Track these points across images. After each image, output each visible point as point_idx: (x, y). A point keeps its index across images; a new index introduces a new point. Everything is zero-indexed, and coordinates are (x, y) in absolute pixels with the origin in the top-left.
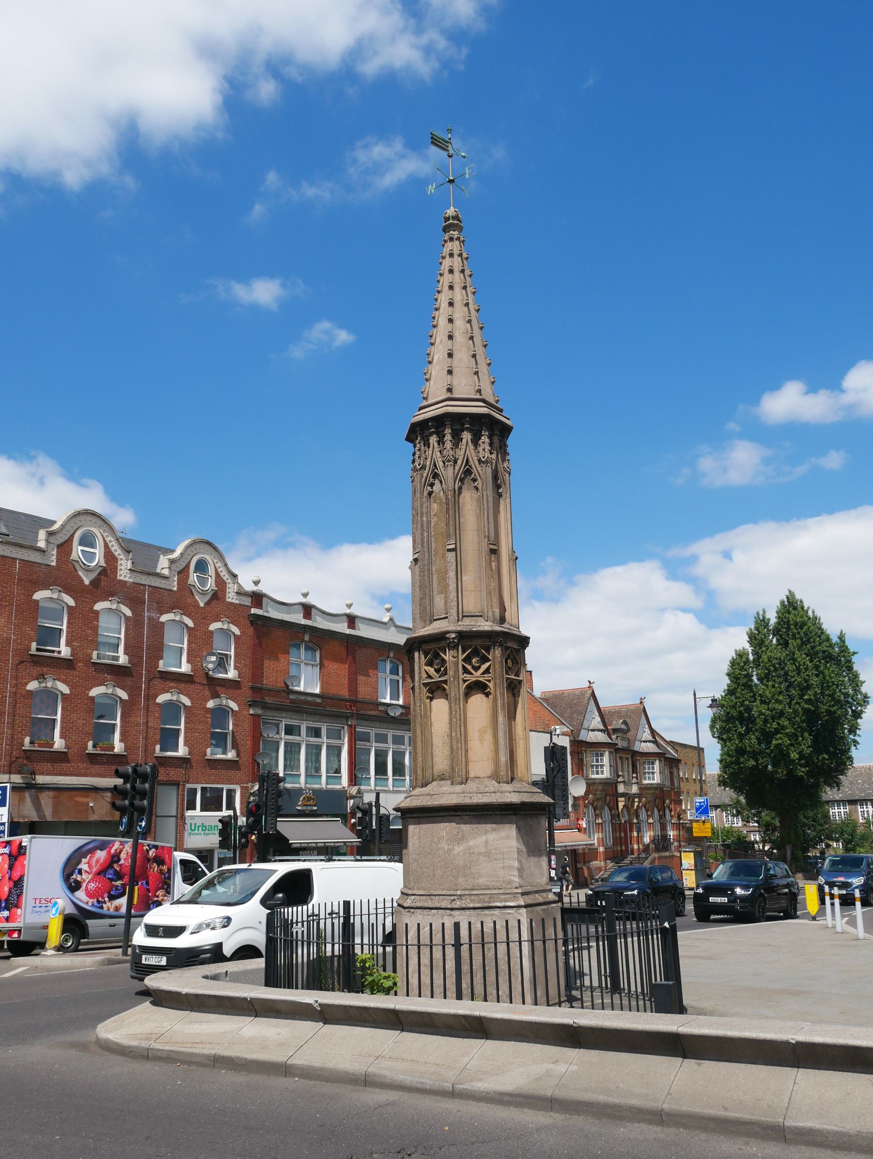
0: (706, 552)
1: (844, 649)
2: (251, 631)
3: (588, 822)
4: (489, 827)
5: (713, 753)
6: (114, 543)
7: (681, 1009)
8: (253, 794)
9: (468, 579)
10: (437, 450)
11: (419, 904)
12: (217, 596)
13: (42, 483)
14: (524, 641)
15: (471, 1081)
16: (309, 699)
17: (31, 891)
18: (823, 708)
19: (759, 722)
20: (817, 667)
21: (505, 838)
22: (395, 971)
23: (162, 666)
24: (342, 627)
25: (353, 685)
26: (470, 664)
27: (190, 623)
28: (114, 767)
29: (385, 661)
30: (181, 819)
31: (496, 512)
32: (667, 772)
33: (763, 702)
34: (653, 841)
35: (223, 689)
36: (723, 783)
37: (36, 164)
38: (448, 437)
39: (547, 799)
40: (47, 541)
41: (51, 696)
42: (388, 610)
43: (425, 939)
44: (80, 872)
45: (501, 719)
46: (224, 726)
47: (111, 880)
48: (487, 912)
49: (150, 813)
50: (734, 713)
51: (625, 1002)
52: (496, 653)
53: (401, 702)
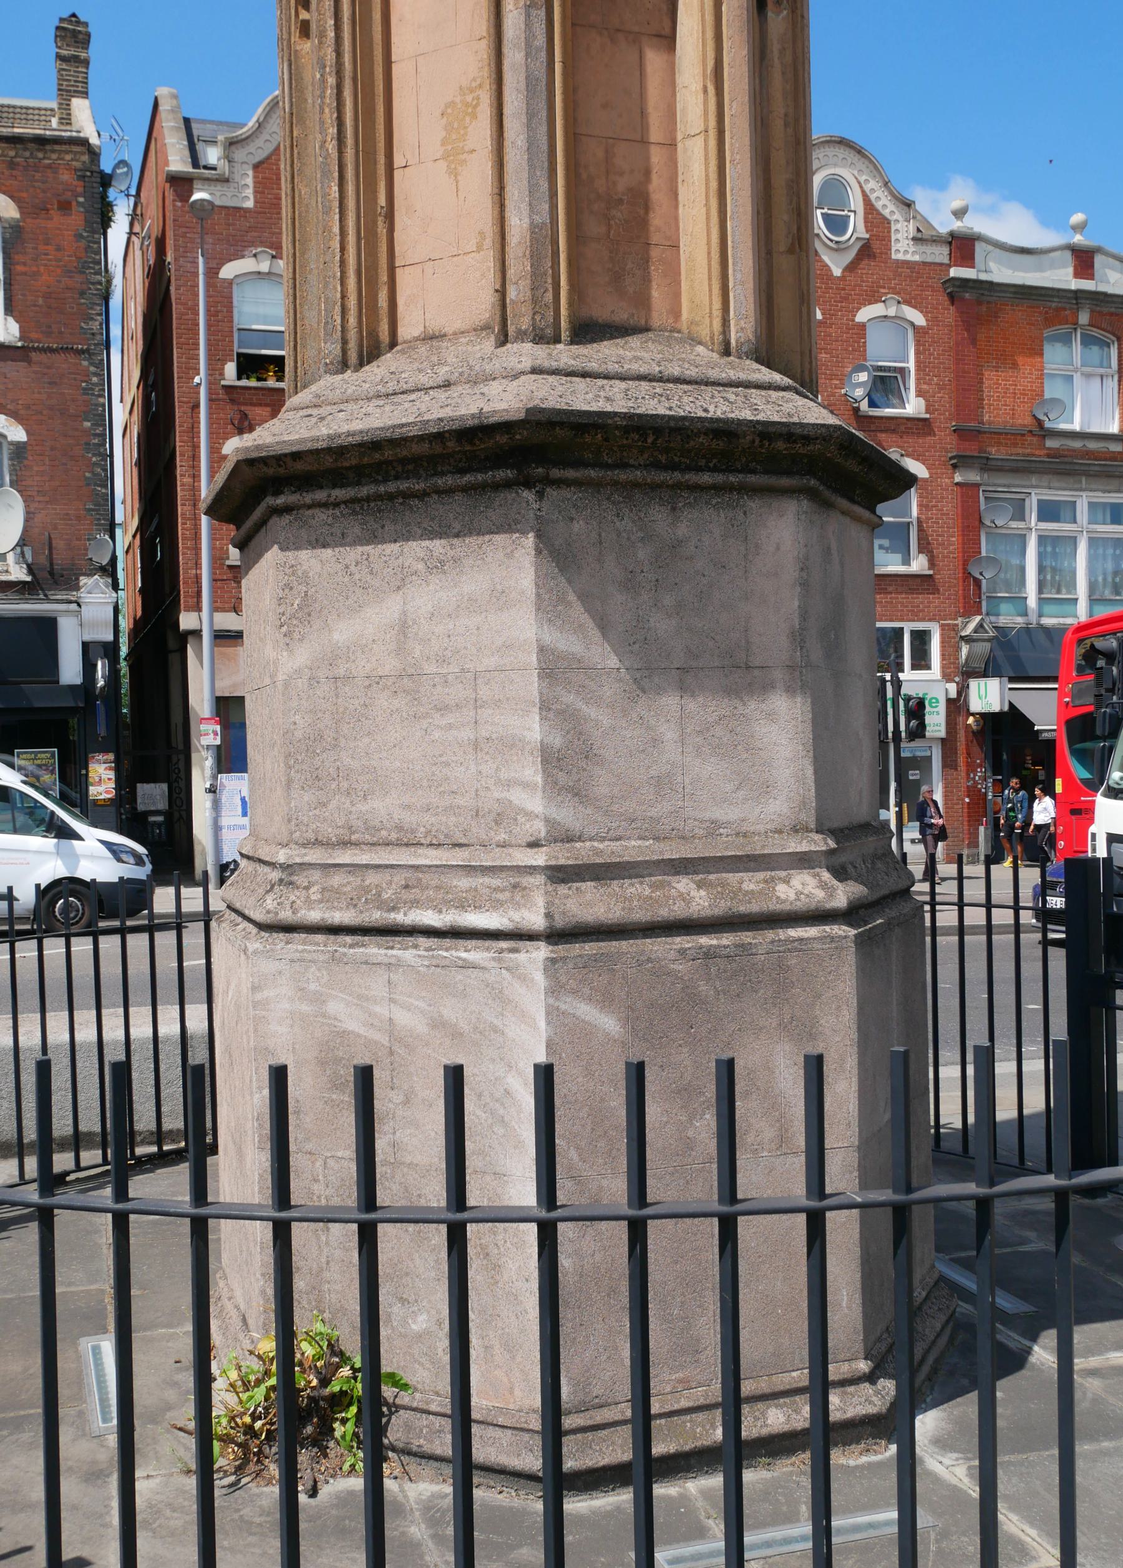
2: (950, 314)
12: (872, 250)
16: (1092, 445)
35: (894, 438)
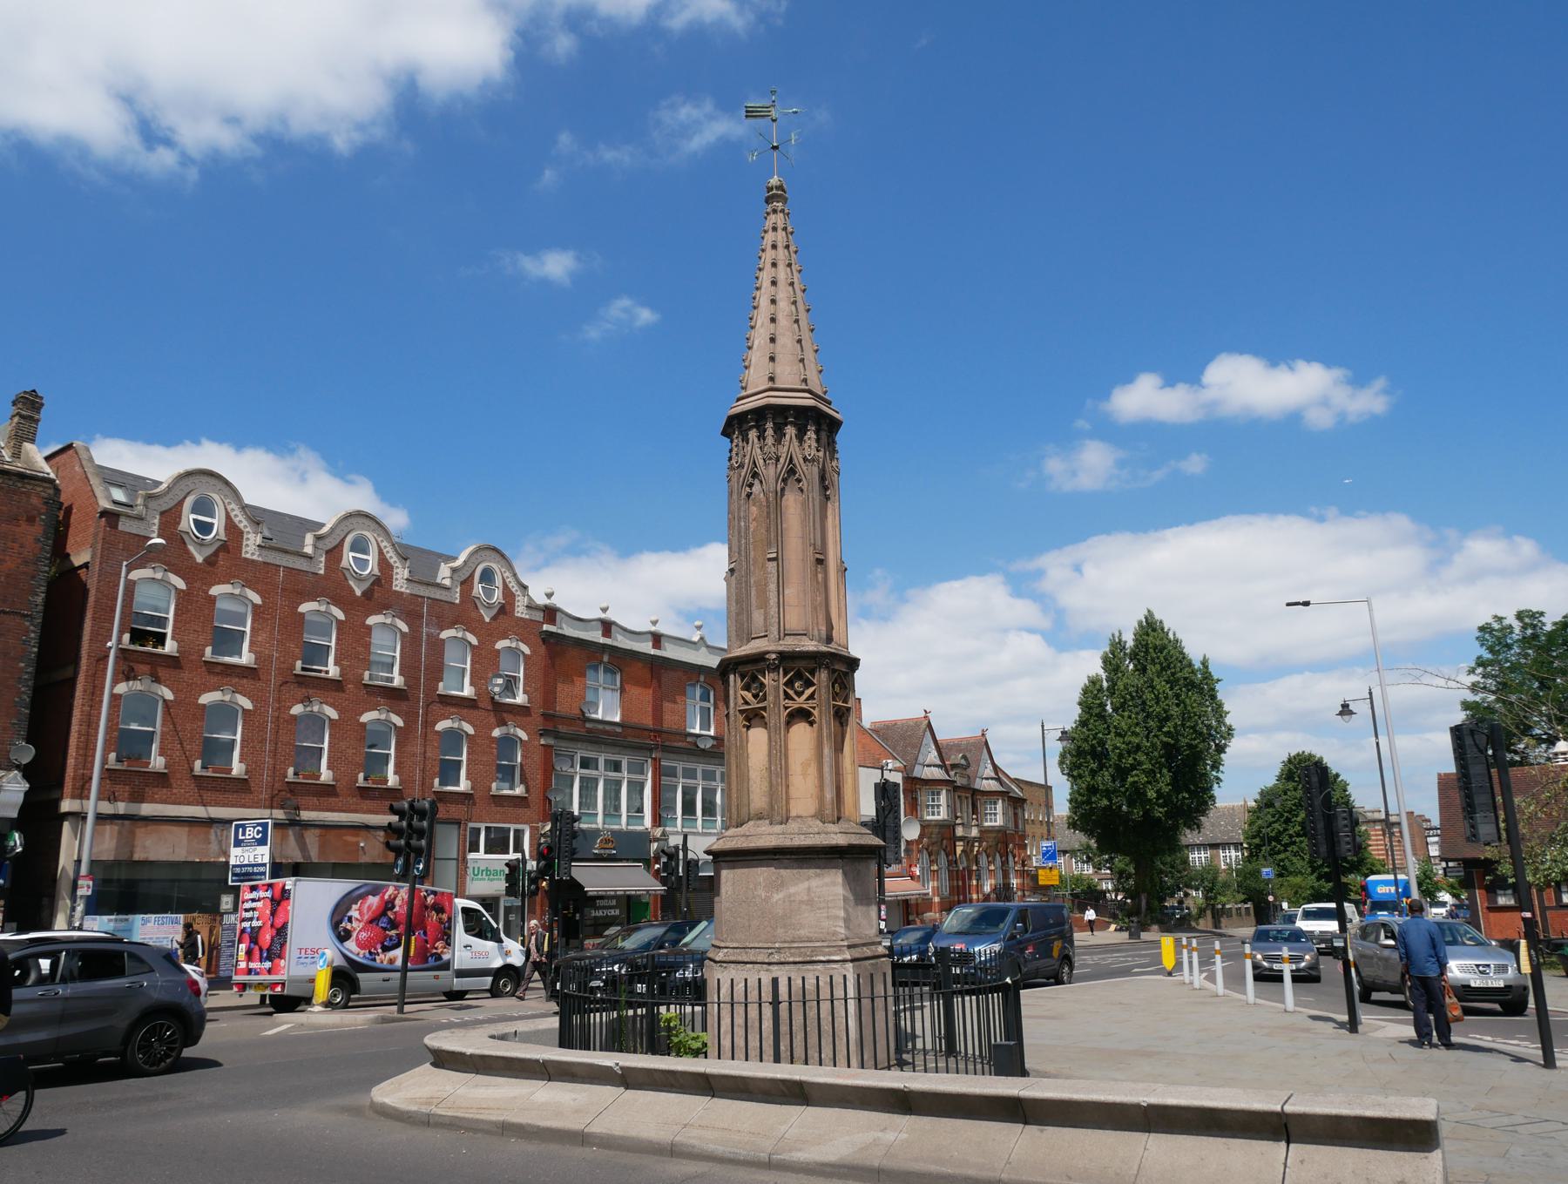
0: (1055, 565)
1: (1207, 676)
2: (542, 650)
3: (922, 869)
4: (811, 872)
5: (1062, 792)
6: (237, 512)
7: (1023, 1073)
8: (544, 835)
9: (791, 592)
10: (757, 445)
11: (732, 958)
12: (505, 610)
13: (303, 479)
14: (853, 663)
15: (790, 1151)
16: (608, 728)
17: (297, 938)
18: (1184, 741)
19: (1114, 757)
20: (1177, 696)
21: (830, 885)
22: (705, 1029)
23: (442, 688)
24: (646, 647)
25: (658, 713)
26: (792, 688)
27: (474, 641)
28: (388, 803)
29: (694, 685)
30: (462, 861)
31: (824, 517)
32: (1011, 813)
33: (1118, 735)
34: (994, 890)
36: (1073, 825)
37: (302, 124)
38: (770, 432)
39: (877, 841)
40: (315, 547)
41: (317, 721)
42: (699, 628)
43: (739, 996)
44: (350, 920)
45: (826, 751)
46: (513, 758)
47: (385, 929)
48: (809, 967)
49: (428, 854)
50: (1086, 747)
51: (962, 1066)
52: (822, 677)
53: (712, 733)
